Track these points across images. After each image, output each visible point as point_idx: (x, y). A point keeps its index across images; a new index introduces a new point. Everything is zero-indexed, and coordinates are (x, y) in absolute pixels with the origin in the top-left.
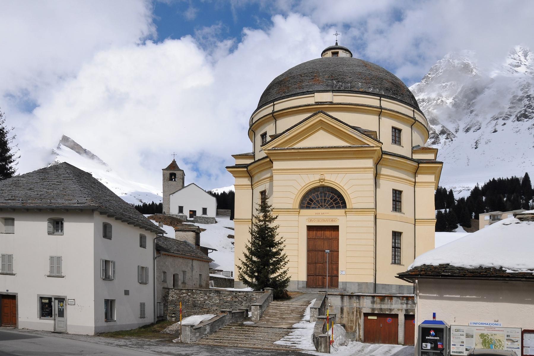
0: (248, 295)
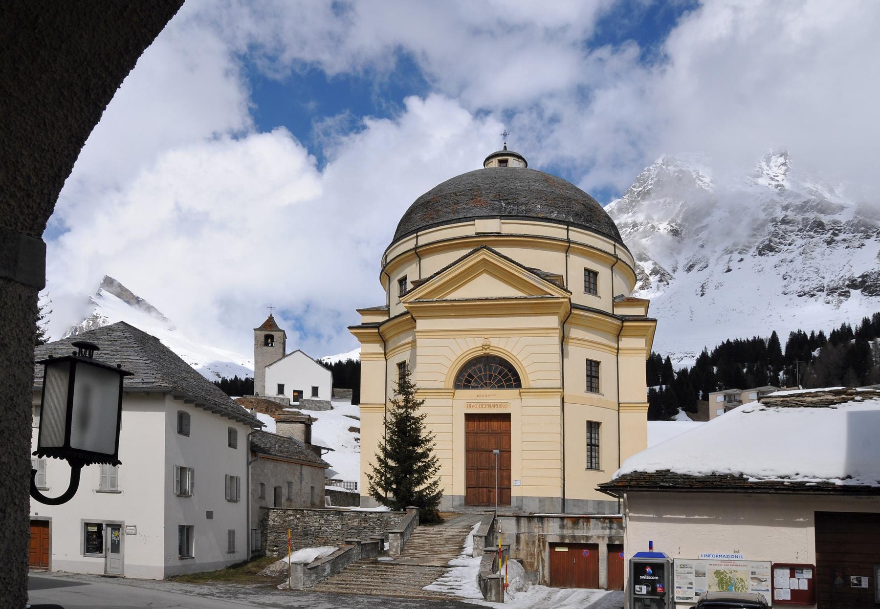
0: (383, 517)
